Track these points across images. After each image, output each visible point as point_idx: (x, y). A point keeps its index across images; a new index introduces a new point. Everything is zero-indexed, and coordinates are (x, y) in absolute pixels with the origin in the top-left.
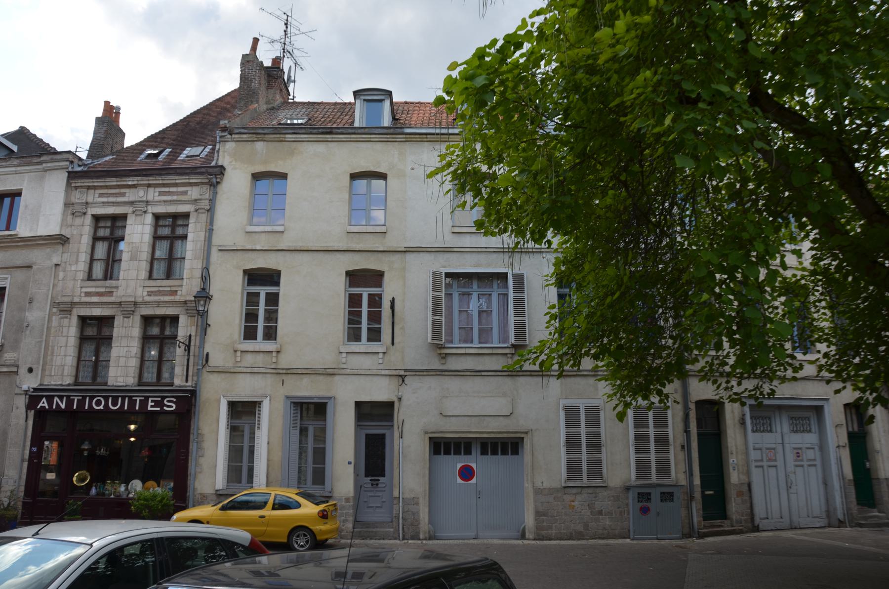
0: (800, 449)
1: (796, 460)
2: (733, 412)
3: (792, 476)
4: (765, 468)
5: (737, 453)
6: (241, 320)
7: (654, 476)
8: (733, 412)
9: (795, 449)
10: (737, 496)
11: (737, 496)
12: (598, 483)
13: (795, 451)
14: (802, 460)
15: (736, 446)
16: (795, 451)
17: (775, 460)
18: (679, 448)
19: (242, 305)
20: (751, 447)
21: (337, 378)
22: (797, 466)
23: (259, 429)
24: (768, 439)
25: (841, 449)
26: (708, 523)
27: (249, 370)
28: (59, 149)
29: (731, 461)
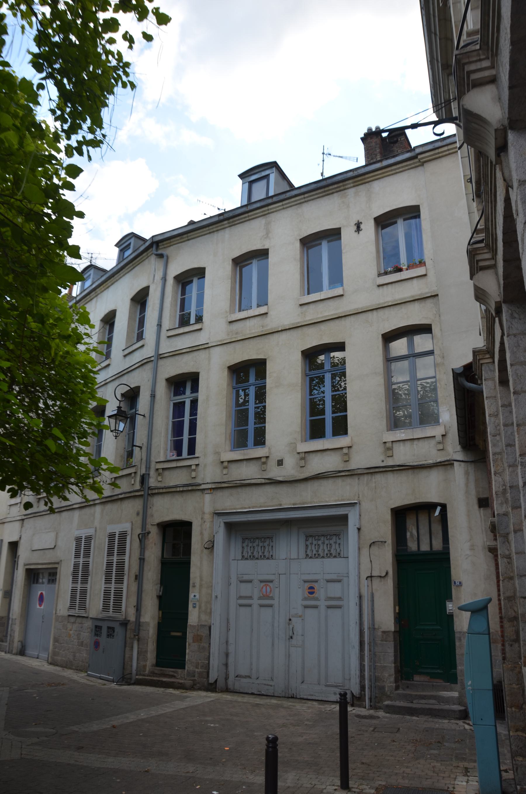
0: (316, 581)
1: (305, 599)
2: (202, 534)
3: (297, 623)
4: (255, 607)
5: (201, 586)
6: (167, 434)
7: (111, 610)
8: (202, 534)
9: (305, 581)
10: (194, 642)
11: (194, 642)
12: (82, 613)
13: (307, 585)
14: (317, 599)
15: (201, 580)
16: (307, 585)
17: (272, 598)
18: (133, 578)
19: (168, 418)
20: (234, 580)
21: (6, 524)
22: (306, 607)
23: (17, 569)
24: (262, 568)
25: (376, 582)
26: (157, 670)
27: (63, 509)
28: (196, 221)
29: (191, 596)
